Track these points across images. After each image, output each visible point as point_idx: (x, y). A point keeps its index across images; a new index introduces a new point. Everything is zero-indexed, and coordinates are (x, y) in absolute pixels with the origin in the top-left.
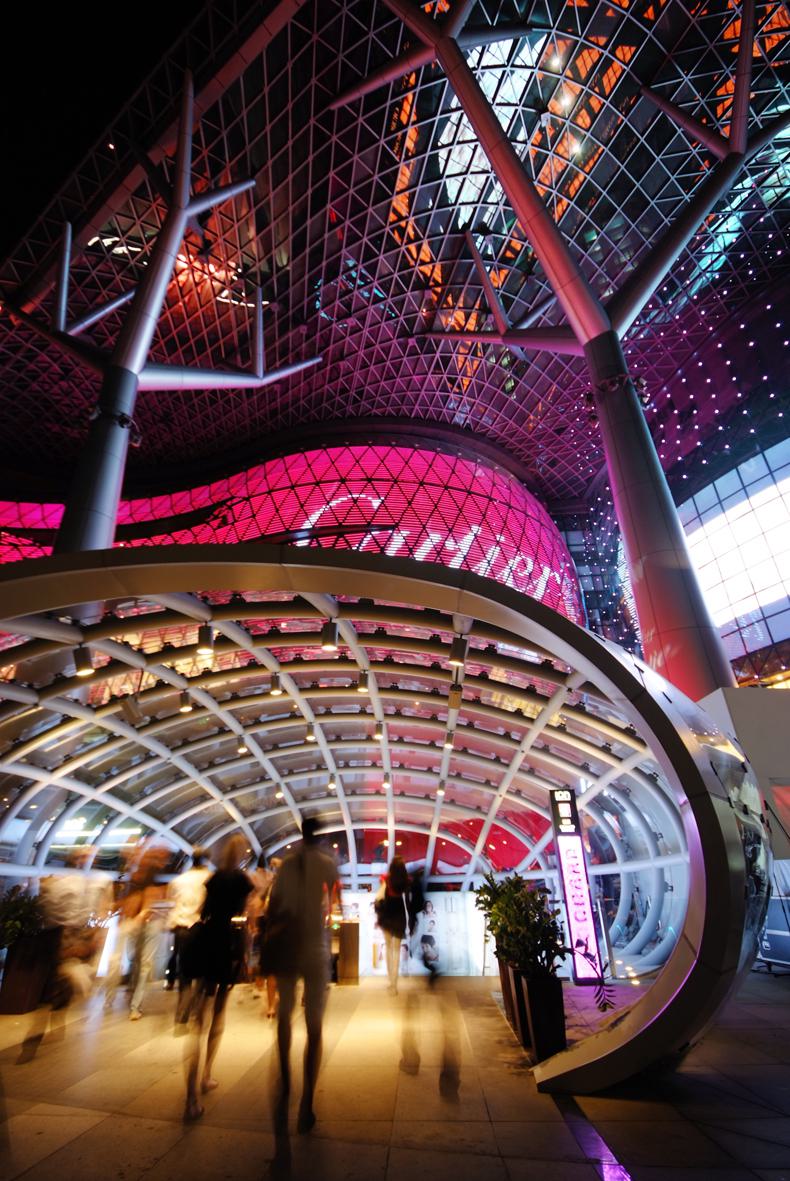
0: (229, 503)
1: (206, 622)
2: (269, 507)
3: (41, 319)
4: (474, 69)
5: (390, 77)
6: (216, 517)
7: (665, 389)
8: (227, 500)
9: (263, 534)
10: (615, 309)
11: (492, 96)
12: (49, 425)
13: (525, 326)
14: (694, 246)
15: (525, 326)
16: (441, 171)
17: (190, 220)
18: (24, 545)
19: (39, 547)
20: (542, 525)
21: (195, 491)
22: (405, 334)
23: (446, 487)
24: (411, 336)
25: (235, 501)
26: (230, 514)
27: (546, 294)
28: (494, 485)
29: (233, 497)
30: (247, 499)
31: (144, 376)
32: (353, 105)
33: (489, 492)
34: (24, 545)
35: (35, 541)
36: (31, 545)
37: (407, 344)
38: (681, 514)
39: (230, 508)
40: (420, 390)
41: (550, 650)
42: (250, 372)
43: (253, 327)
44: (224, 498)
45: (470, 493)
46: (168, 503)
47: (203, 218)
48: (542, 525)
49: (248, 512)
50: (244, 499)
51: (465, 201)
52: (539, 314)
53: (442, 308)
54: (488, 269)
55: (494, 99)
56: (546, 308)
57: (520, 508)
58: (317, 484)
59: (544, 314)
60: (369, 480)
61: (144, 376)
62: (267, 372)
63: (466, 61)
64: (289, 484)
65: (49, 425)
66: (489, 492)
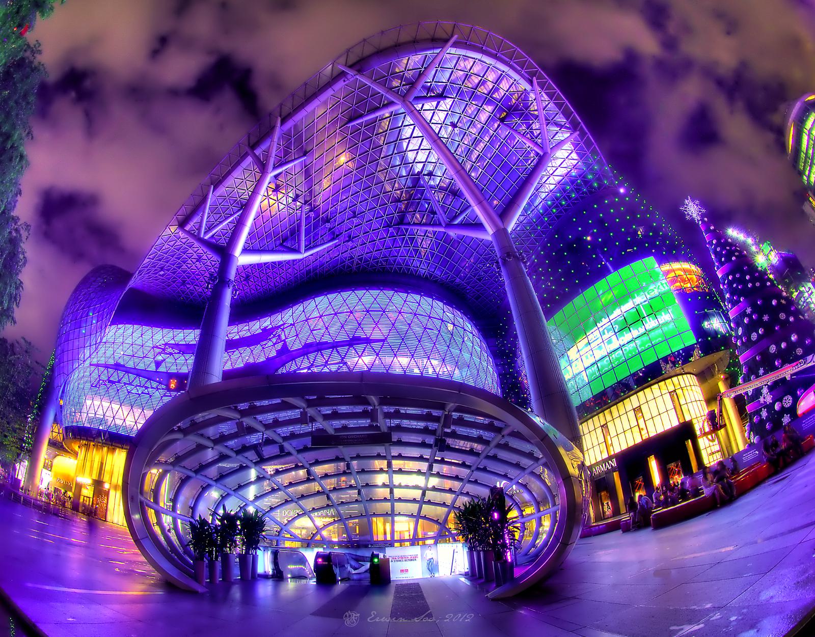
0: (282, 327)
1: (239, 419)
2: (306, 329)
3: (193, 232)
4: (420, 110)
5: (378, 114)
6: (274, 336)
7: (533, 257)
8: (281, 325)
9: (334, 340)
10: (504, 213)
11: (430, 119)
12: (188, 286)
13: (456, 222)
14: (537, 189)
15: (456, 222)
16: (405, 149)
17: (271, 177)
18: (175, 353)
19: (182, 355)
20: (473, 335)
21: (251, 324)
22: (388, 226)
23: (430, 317)
24: (391, 227)
25: (286, 326)
26: (283, 334)
27: (466, 206)
28: (444, 312)
29: (285, 324)
30: (293, 325)
31: (242, 259)
32: (361, 124)
33: (441, 315)
34: (175, 353)
35: (180, 351)
36: (178, 353)
37: (389, 231)
38: (553, 328)
39: (283, 330)
40: (397, 256)
42: (297, 251)
43: (300, 223)
44: (279, 324)
45: (430, 317)
46: (171, 335)
47: (276, 177)
48: (473, 335)
49: (293, 333)
50: (291, 324)
51: (415, 136)
52: (464, 215)
53: (408, 212)
54: (433, 192)
55: (430, 121)
56: (467, 213)
57: (469, 331)
58: (336, 314)
59: (466, 216)
60: (368, 311)
61: (242, 259)
62: (306, 251)
63: (419, 276)
64: (318, 315)
65: (188, 286)
66: (441, 315)
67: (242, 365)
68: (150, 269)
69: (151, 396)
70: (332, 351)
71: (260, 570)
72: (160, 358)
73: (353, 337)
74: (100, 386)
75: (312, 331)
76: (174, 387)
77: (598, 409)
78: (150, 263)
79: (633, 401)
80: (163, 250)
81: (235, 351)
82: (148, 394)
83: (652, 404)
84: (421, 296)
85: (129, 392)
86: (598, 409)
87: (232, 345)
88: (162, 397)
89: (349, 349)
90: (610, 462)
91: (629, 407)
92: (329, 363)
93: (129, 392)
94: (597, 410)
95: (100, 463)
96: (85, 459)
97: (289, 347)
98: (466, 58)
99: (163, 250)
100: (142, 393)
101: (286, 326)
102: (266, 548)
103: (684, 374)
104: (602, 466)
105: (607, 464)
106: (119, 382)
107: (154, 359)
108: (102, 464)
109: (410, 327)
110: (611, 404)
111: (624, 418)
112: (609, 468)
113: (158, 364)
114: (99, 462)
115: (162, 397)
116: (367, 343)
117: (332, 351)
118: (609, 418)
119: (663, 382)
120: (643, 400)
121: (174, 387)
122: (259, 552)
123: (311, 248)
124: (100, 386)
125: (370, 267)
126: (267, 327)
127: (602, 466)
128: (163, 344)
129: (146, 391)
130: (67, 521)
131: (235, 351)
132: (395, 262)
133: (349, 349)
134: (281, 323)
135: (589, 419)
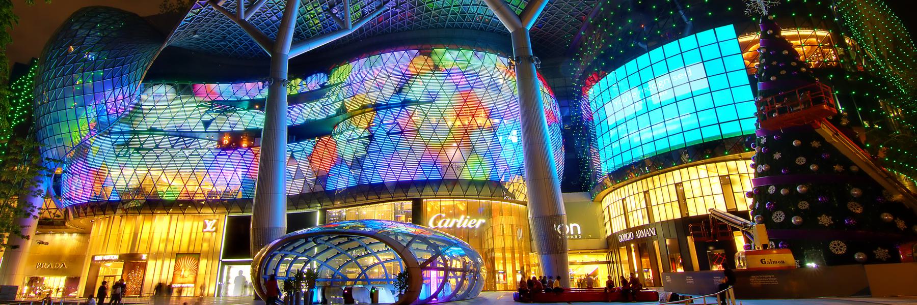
40: (445, 22)
41: (128, 303)
50: (348, 84)
68: (200, 18)
69: (202, 157)
70: (386, 112)
72: (207, 118)
73: (405, 99)
74: (130, 155)
75: (367, 93)
76: (228, 142)
77: (661, 169)
80: (187, 18)
81: (294, 107)
82: (199, 155)
85: (173, 157)
86: (661, 169)
87: (294, 100)
88: (216, 157)
89: (401, 110)
90: (650, 229)
92: (384, 122)
93: (173, 157)
94: (659, 169)
95: (132, 234)
96: (106, 234)
97: (347, 107)
98: (178, 33)
100: (191, 155)
104: (643, 231)
105: (647, 230)
107: (201, 119)
108: (136, 235)
110: (647, 175)
112: (649, 235)
114: (131, 233)
115: (216, 157)
116: (417, 105)
117: (386, 112)
118: (651, 186)
121: (228, 142)
124: (130, 155)
125: (431, 24)
126: (325, 83)
127: (643, 231)
128: (209, 102)
129: (195, 153)
130: (324, 182)
131: (294, 107)
133: (401, 110)
134: (339, 81)
135: (662, 173)
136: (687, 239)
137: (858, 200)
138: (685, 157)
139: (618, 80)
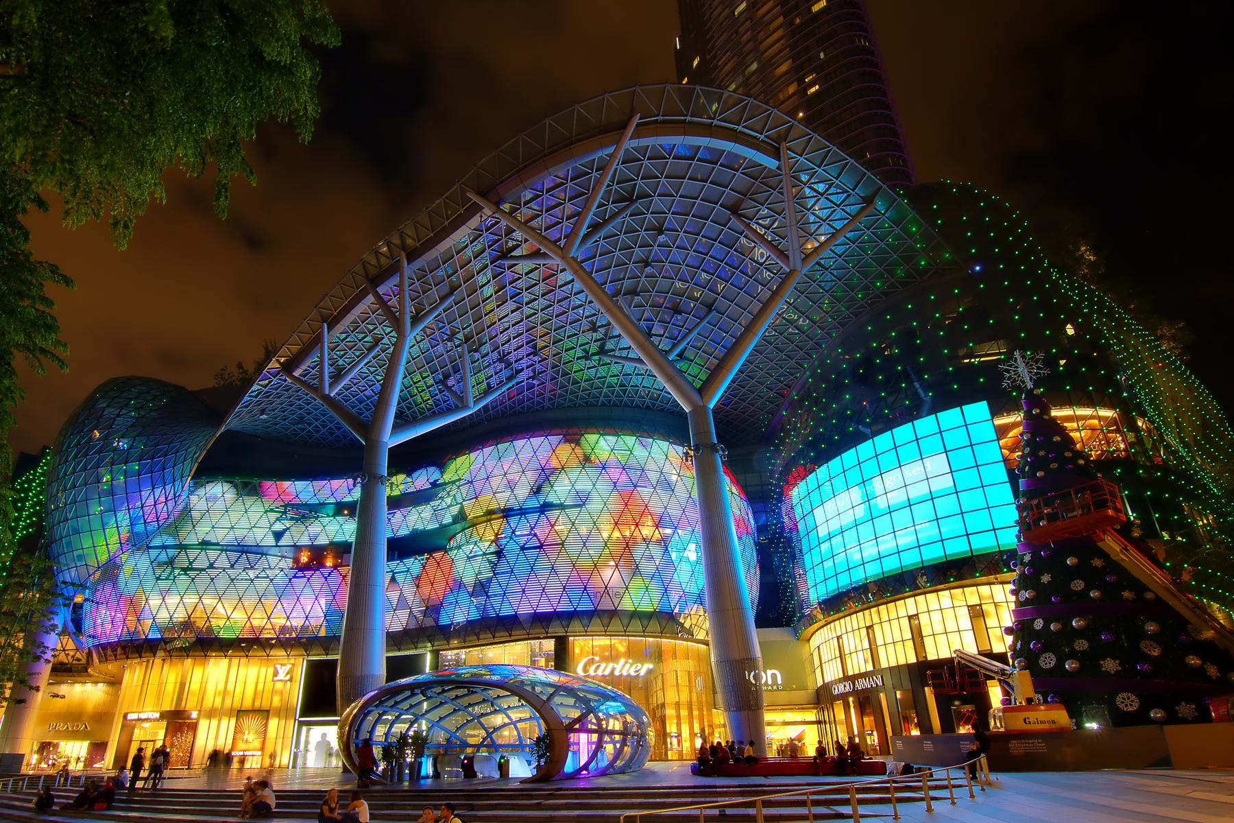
25: (462, 482)
50: (469, 482)
67: (407, 532)
69: (271, 580)
70: (520, 519)
71: (423, 773)
74: (175, 577)
75: (494, 493)
78: (249, 405)
79: (909, 605)
82: (268, 577)
83: (936, 616)
84: (619, 436)
87: (396, 503)
89: (540, 516)
91: (902, 612)
92: (517, 533)
95: (178, 684)
96: (143, 684)
97: (467, 512)
99: (274, 384)
100: (257, 577)
101: (462, 482)
102: (428, 756)
103: (994, 583)
106: (211, 566)
107: (270, 528)
108: (182, 685)
109: (615, 486)
111: (895, 623)
113: (278, 535)
114: (176, 683)
115: (290, 579)
117: (520, 519)
119: (960, 590)
120: (922, 608)
121: (306, 560)
122: (423, 760)
123: (30, 789)
124: (175, 577)
126: (437, 480)
132: (589, 396)
133: (540, 516)
134: (456, 477)
136: (924, 691)
137: (1155, 638)
138: (922, 581)
139: (824, 501)
